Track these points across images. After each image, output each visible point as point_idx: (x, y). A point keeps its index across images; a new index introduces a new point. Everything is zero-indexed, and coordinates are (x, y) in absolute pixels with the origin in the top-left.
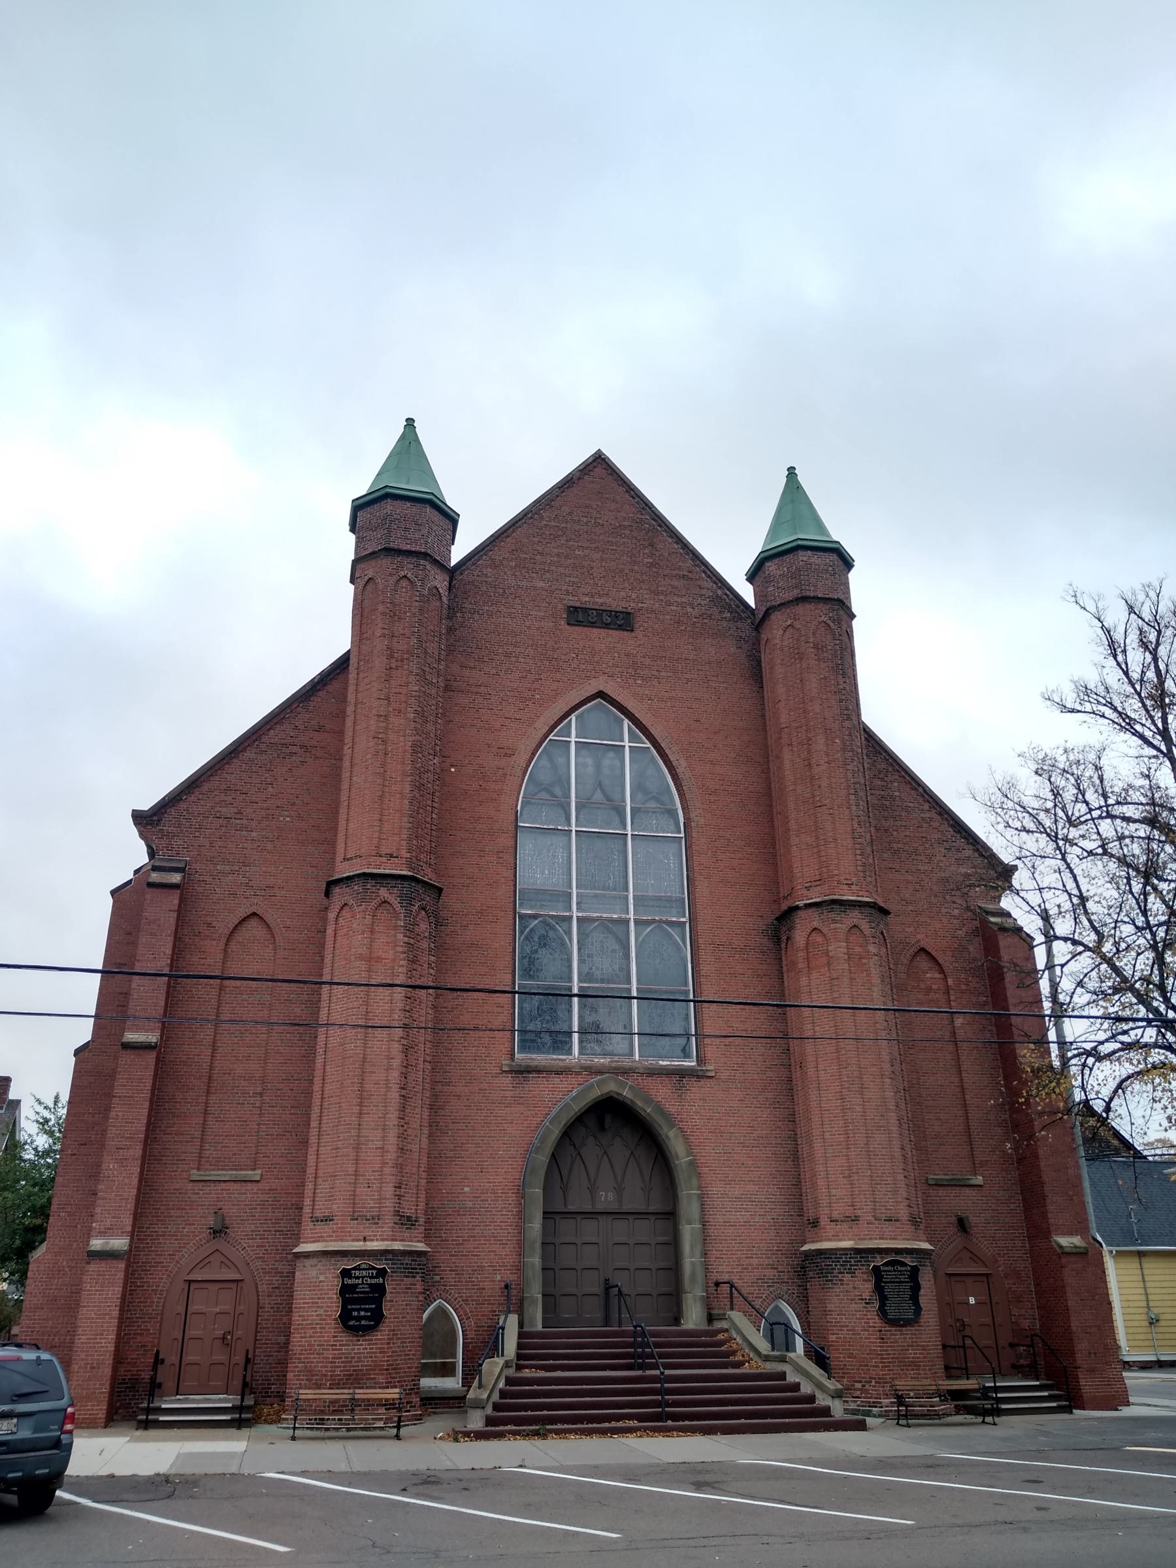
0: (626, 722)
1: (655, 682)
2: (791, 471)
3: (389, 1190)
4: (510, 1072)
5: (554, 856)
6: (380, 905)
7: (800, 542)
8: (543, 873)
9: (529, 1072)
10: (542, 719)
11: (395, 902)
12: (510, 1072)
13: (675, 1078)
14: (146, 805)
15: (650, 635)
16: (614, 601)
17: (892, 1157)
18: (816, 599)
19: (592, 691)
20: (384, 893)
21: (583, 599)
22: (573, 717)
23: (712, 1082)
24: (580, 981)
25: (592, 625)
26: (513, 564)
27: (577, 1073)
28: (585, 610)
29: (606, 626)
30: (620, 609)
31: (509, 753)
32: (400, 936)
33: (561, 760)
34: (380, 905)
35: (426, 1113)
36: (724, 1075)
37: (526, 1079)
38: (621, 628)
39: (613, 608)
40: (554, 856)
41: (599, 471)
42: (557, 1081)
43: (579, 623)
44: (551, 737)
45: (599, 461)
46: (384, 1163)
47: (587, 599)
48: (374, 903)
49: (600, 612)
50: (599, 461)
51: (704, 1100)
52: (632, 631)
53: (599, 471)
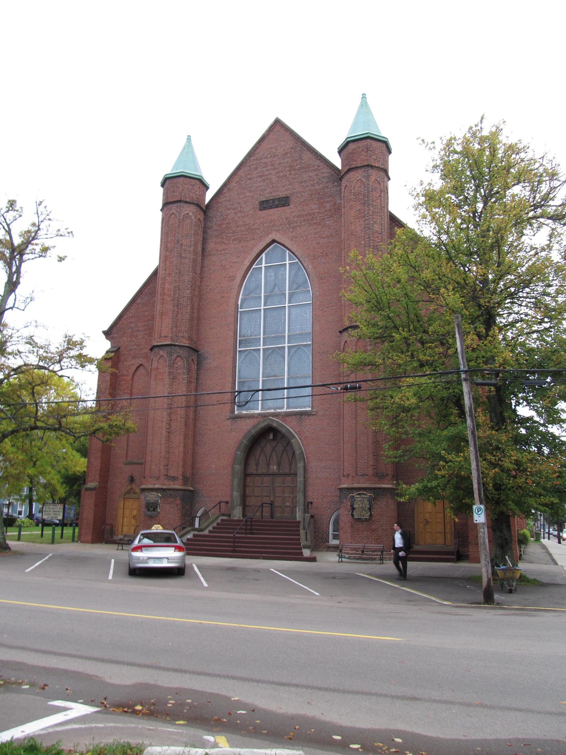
0: (287, 251)
1: (299, 229)
2: (364, 96)
3: (162, 467)
4: (230, 419)
5: (256, 322)
6: (160, 358)
7: (348, 140)
8: (251, 330)
9: (238, 418)
10: (247, 260)
11: (165, 355)
12: (230, 419)
13: (298, 417)
14: (106, 328)
15: (297, 205)
16: (282, 194)
17: (368, 447)
18: (357, 168)
19: (268, 240)
20: (161, 353)
21: (267, 195)
22: (263, 255)
23: (315, 417)
24: (263, 377)
25: (271, 208)
26: (237, 188)
27: (257, 418)
28: (267, 201)
29: (277, 206)
30: (284, 196)
31: (233, 278)
32: (167, 369)
33: (260, 276)
34: (160, 358)
35: (182, 438)
36: (320, 413)
37: (236, 421)
38: (284, 205)
39: (281, 196)
40: (256, 322)
41: (278, 128)
42: (248, 421)
43: (265, 209)
44: (254, 267)
45: (278, 123)
46: (161, 457)
47: (269, 195)
48: (158, 357)
49: (273, 200)
50: (278, 123)
51: (311, 425)
52: (289, 205)
53: (278, 128)
